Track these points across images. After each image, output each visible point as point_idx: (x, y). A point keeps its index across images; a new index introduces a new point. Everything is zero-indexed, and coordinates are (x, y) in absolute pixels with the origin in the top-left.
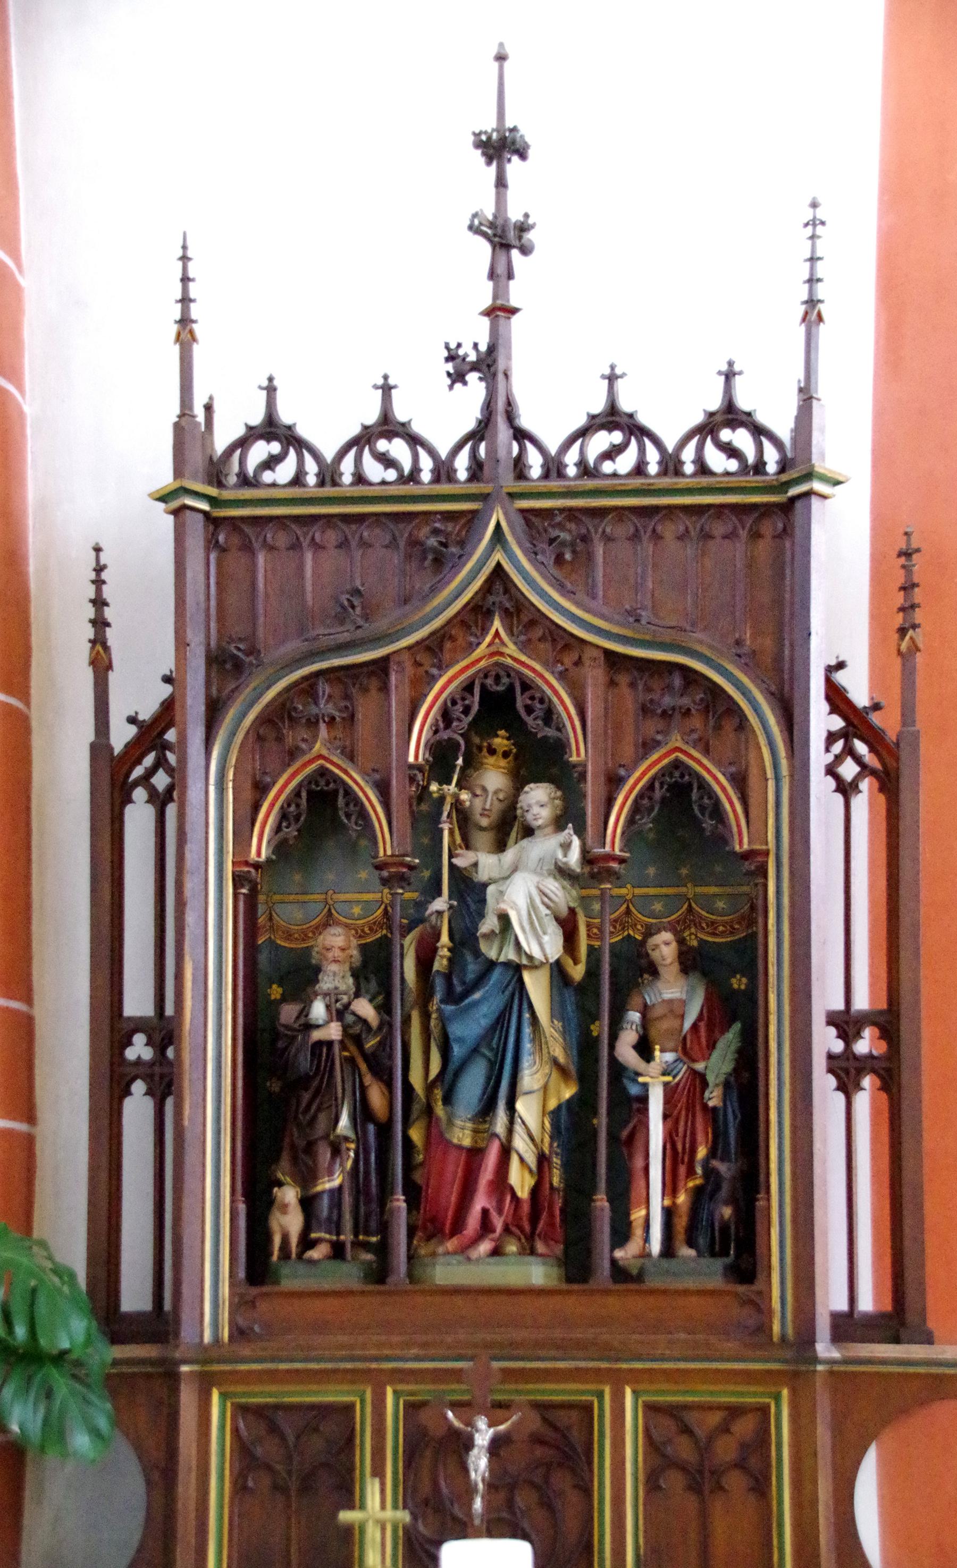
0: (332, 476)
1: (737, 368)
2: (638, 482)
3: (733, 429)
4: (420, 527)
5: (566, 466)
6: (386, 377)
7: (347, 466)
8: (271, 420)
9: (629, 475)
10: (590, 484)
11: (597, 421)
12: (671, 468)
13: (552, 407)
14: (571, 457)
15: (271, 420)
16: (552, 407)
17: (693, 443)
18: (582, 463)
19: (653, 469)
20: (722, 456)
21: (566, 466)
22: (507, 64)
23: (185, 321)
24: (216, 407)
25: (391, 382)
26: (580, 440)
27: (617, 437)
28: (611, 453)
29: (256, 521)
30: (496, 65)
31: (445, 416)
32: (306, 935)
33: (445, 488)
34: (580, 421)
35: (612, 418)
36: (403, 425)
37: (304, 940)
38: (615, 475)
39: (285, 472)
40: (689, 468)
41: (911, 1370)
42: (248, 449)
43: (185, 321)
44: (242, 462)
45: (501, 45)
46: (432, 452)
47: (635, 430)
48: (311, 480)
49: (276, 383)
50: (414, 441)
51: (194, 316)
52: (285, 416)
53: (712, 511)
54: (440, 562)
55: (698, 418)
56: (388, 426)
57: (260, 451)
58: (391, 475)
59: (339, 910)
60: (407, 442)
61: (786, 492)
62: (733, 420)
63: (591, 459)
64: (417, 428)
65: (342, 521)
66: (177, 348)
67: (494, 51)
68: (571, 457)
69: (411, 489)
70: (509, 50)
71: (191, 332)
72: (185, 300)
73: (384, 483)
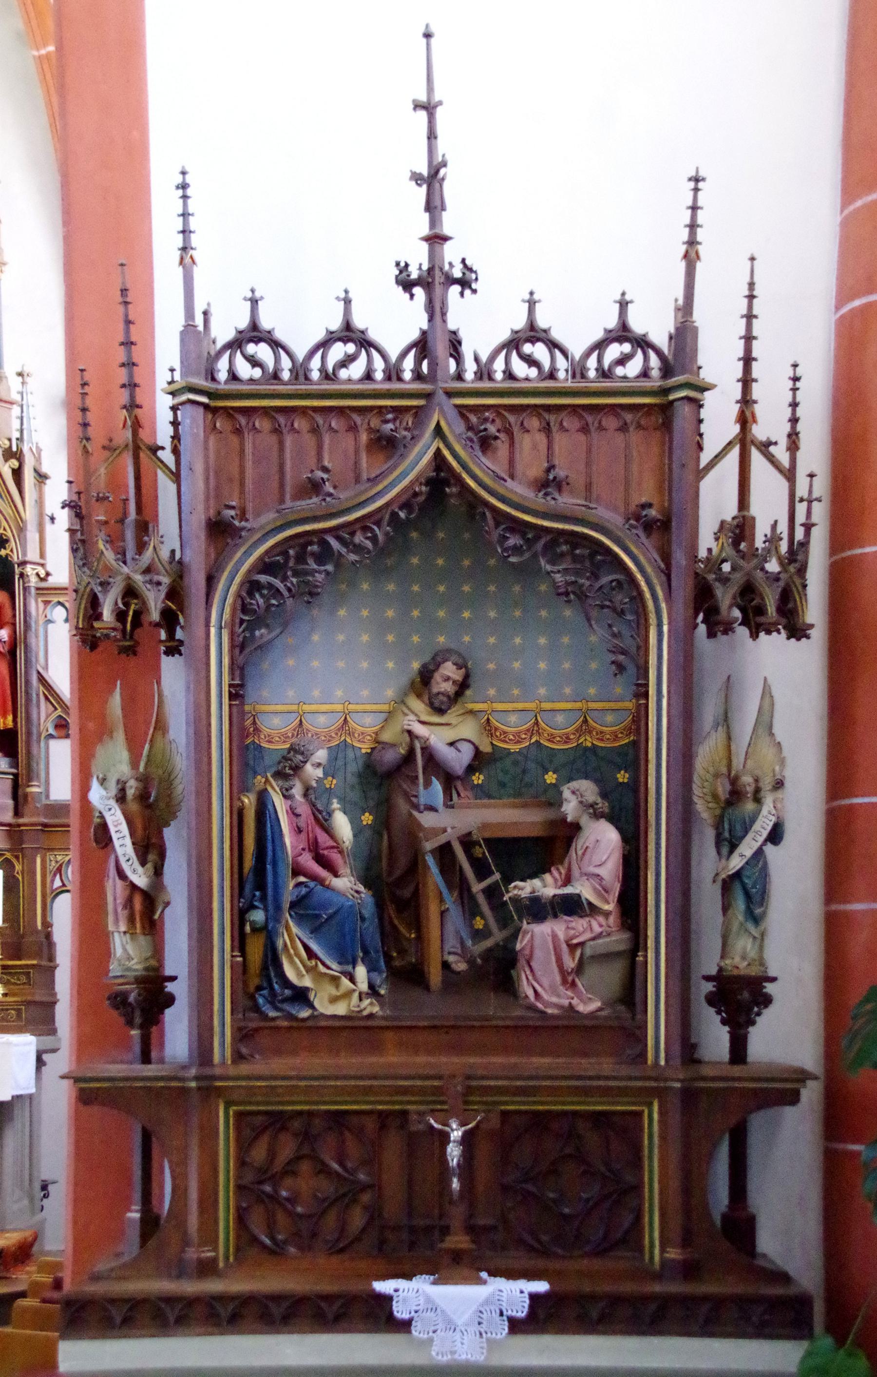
0: (581, 370)
1: (536, 297)
2: (368, 386)
3: (533, 343)
4: (382, 417)
5: (312, 370)
6: (531, 293)
7: (499, 365)
8: (348, 326)
9: (361, 380)
10: (607, 384)
11: (614, 335)
12: (301, 373)
13: (480, 325)
14: (315, 363)
15: (348, 326)
16: (480, 325)
17: (595, 355)
18: (323, 370)
19: (379, 375)
20: (248, 366)
21: (312, 370)
22: (433, 41)
23: (692, 242)
24: (213, 310)
25: (258, 294)
26: (228, 353)
27: (351, 348)
28: (622, 361)
29: (247, 411)
30: (424, 40)
31: (395, 323)
32: (616, 736)
33: (486, 385)
34: (599, 335)
35: (348, 332)
36: (545, 331)
37: (615, 740)
38: (625, 377)
39: (356, 370)
40: (499, 376)
41: (557, 1083)
42: (329, 348)
43: (692, 242)
44: (323, 358)
45: (427, 26)
46: (384, 356)
47: (365, 343)
48: (379, 375)
49: (351, 295)
50: (553, 345)
51: (699, 239)
52: (359, 323)
53: (646, 409)
54: (387, 446)
55: (505, 335)
56: (533, 333)
57: (338, 351)
58: (257, 373)
59: (596, 719)
60: (270, 345)
61: (667, 396)
62: (534, 337)
63: (330, 367)
64: (279, 335)
65: (313, 411)
66: (683, 264)
67: (422, 30)
68: (592, 363)
69: (550, 384)
70: (433, 29)
71: (697, 253)
72: (693, 226)
73: (527, 379)
